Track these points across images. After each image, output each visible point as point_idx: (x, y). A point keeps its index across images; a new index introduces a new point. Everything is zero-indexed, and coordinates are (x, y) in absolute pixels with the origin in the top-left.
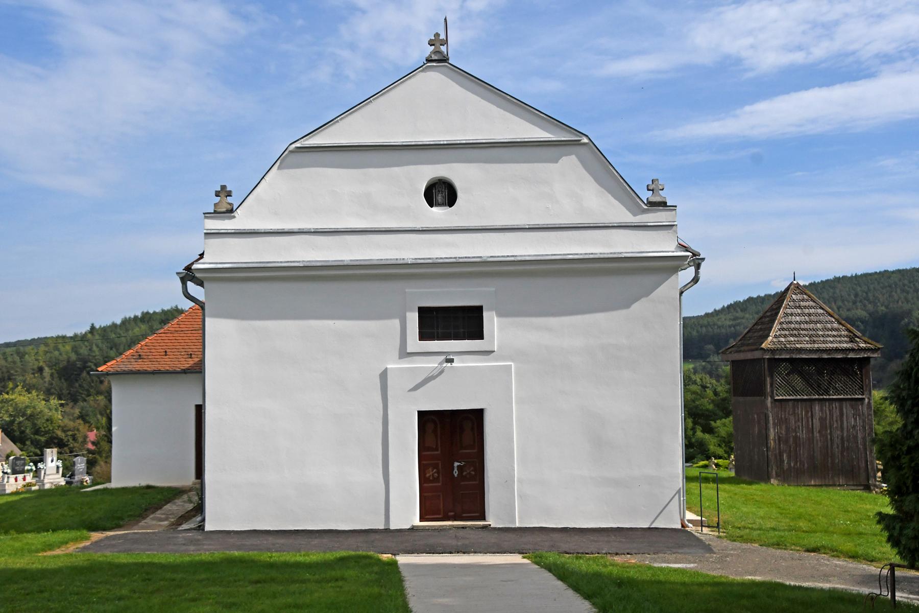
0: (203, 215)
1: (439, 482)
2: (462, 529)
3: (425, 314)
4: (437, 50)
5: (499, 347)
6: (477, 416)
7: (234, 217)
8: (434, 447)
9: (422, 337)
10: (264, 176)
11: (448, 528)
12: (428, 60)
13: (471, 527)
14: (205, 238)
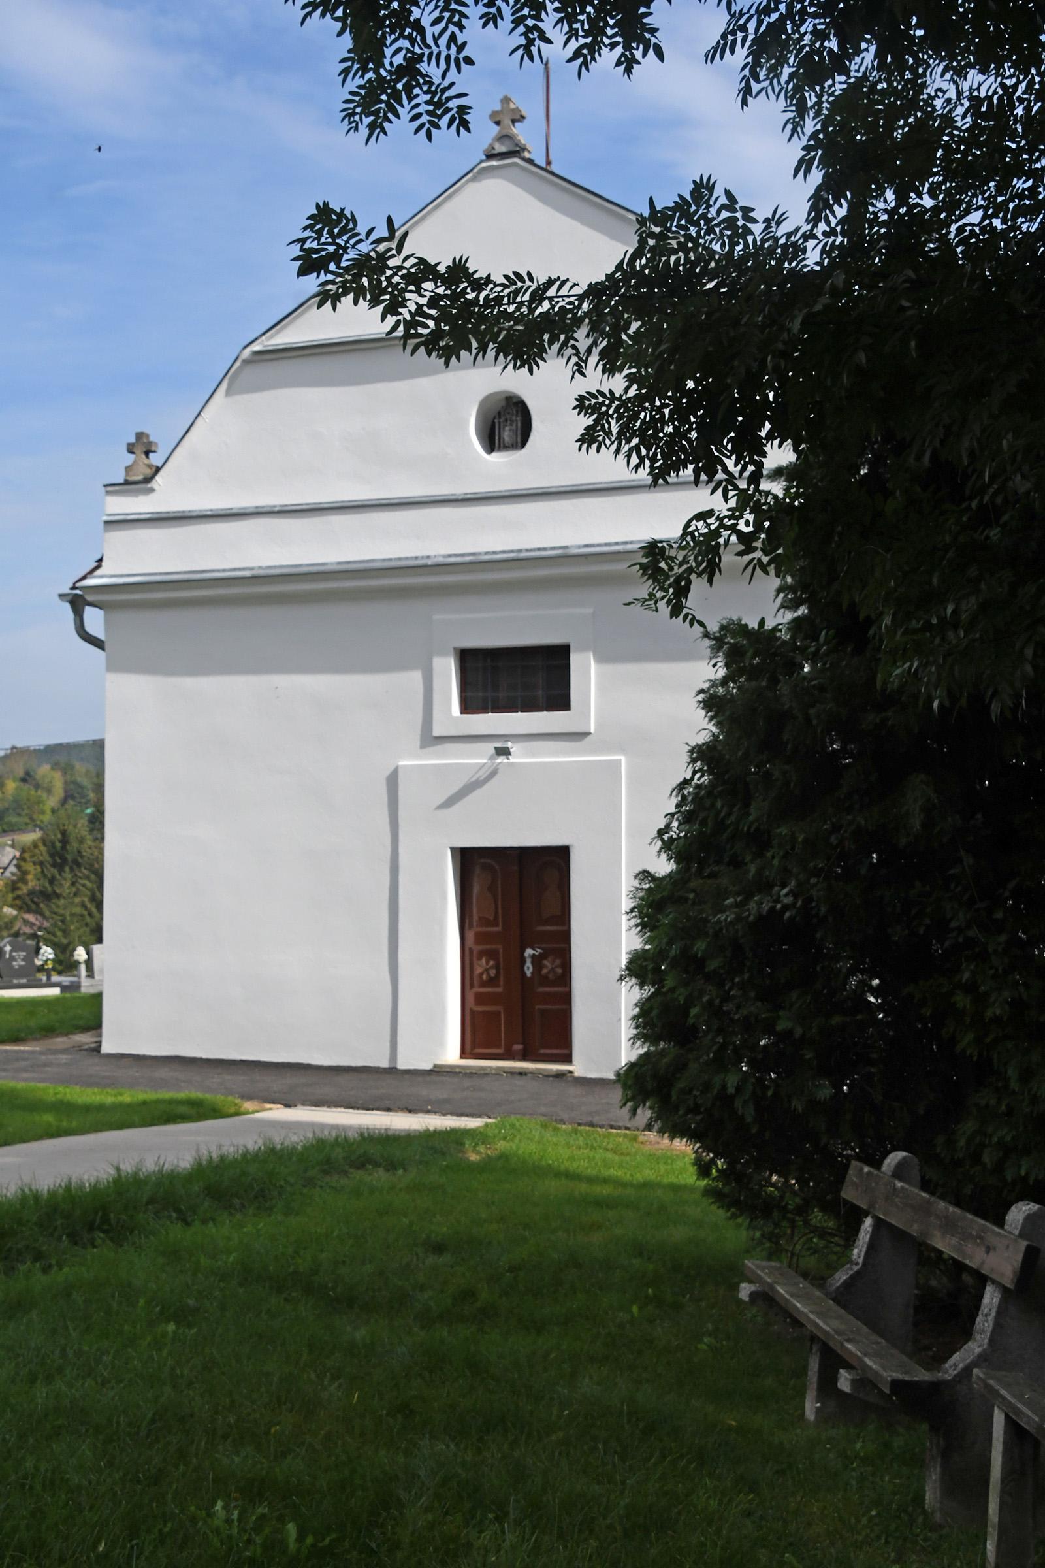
0: (103, 488)
1: (498, 986)
2: (518, 1077)
3: (469, 660)
4: (505, 132)
5: (599, 725)
6: (558, 858)
7: (152, 490)
8: (492, 918)
9: (466, 708)
10: (201, 410)
11: (493, 1072)
12: (490, 156)
13: (534, 1074)
14: (106, 531)
